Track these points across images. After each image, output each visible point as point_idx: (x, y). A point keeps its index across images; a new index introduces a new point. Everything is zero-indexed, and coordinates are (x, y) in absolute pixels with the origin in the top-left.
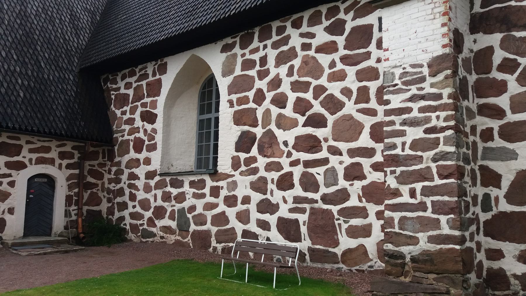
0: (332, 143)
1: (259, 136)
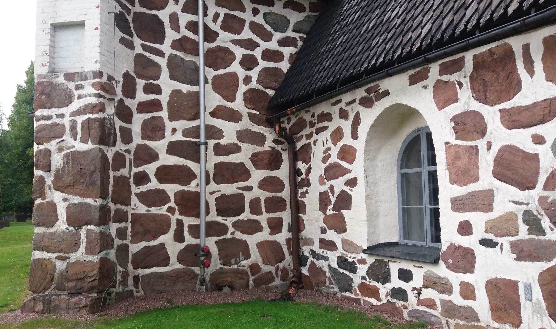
0: (163, 210)
1: (216, 238)
